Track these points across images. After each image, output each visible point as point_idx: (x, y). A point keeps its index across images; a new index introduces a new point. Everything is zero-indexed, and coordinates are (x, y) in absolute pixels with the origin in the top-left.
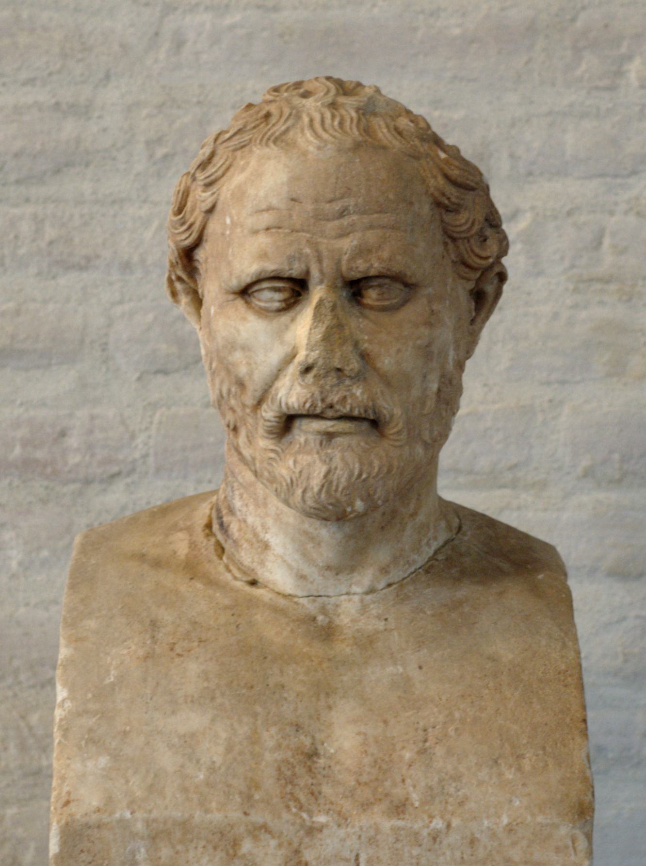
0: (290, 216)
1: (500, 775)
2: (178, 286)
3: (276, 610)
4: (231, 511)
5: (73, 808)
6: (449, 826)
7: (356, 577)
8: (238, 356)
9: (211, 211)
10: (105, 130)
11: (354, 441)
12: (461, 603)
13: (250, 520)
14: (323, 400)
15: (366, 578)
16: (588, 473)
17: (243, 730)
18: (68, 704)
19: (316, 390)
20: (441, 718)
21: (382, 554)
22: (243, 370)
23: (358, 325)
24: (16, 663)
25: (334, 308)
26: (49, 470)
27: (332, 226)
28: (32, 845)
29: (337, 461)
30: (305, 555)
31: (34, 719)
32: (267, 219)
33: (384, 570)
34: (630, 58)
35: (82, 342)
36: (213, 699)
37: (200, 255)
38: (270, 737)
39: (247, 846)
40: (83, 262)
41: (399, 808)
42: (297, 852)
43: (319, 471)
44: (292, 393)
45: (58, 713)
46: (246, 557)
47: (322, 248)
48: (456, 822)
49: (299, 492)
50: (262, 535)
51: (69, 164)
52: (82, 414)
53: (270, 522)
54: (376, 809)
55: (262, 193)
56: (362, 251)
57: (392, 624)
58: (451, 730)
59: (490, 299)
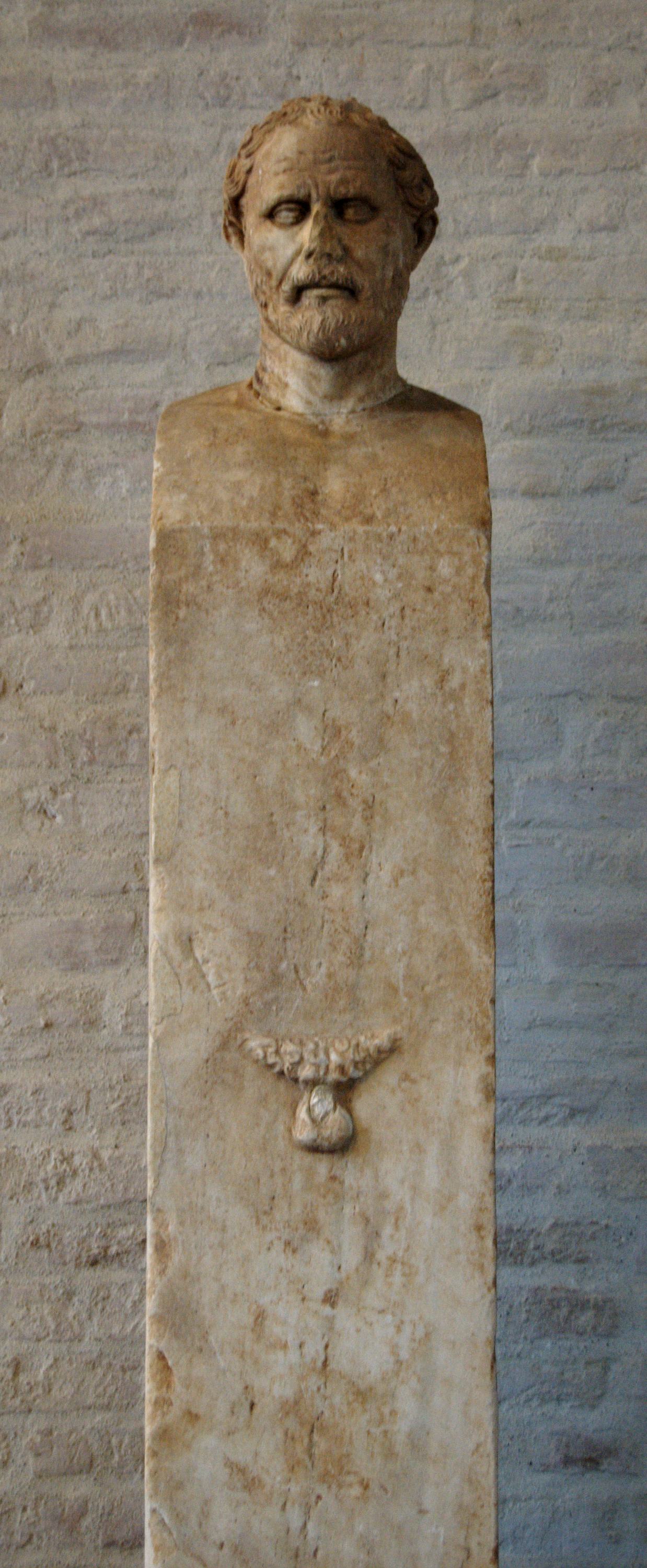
0: (299, 162)
1: (432, 502)
2: (230, 230)
3: (292, 421)
4: (264, 369)
5: (164, 521)
6: (400, 530)
7: (343, 403)
8: (267, 255)
9: (249, 171)
10: (184, 207)
11: (339, 302)
12: (410, 419)
13: (276, 370)
14: (319, 273)
15: (349, 403)
16: (508, 427)
17: (271, 479)
18: (161, 470)
19: (315, 268)
20: (396, 473)
21: (360, 389)
22: (270, 264)
23: (341, 229)
24: (125, 556)
25: (326, 217)
26: (147, 428)
27: (324, 168)
28: (136, 676)
29: (329, 313)
30: (311, 389)
31: (137, 593)
32: (284, 165)
33: (361, 400)
34: (532, 156)
35: (169, 345)
36: (252, 463)
37: (244, 201)
38: (287, 483)
39: (273, 543)
40: (169, 292)
41: (369, 520)
42: (305, 546)
43: (318, 319)
44: (300, 271)
45: (155, 475)
46: (273, 394)
47: (319, 181)
48: (404, 528)
49: (305, 334)
50: (283, 378)
51: (160, 229)
52: (169, 392)
53: (288, 370)
54: (354, 520)
55: (281, 151)
56: (343, 182)
57: (365, 427)
58: (402, 479)
59: (428, 234)
